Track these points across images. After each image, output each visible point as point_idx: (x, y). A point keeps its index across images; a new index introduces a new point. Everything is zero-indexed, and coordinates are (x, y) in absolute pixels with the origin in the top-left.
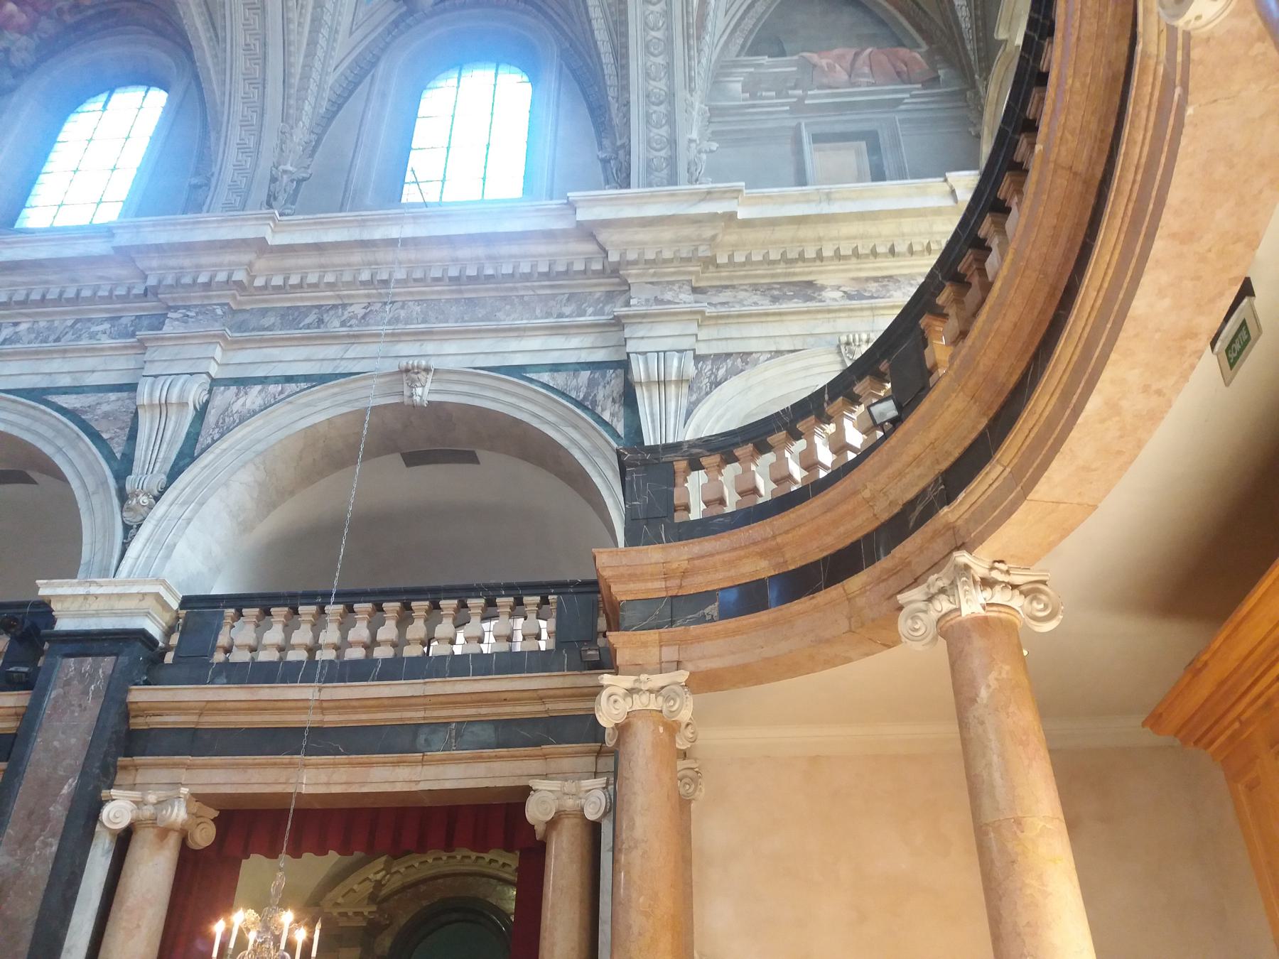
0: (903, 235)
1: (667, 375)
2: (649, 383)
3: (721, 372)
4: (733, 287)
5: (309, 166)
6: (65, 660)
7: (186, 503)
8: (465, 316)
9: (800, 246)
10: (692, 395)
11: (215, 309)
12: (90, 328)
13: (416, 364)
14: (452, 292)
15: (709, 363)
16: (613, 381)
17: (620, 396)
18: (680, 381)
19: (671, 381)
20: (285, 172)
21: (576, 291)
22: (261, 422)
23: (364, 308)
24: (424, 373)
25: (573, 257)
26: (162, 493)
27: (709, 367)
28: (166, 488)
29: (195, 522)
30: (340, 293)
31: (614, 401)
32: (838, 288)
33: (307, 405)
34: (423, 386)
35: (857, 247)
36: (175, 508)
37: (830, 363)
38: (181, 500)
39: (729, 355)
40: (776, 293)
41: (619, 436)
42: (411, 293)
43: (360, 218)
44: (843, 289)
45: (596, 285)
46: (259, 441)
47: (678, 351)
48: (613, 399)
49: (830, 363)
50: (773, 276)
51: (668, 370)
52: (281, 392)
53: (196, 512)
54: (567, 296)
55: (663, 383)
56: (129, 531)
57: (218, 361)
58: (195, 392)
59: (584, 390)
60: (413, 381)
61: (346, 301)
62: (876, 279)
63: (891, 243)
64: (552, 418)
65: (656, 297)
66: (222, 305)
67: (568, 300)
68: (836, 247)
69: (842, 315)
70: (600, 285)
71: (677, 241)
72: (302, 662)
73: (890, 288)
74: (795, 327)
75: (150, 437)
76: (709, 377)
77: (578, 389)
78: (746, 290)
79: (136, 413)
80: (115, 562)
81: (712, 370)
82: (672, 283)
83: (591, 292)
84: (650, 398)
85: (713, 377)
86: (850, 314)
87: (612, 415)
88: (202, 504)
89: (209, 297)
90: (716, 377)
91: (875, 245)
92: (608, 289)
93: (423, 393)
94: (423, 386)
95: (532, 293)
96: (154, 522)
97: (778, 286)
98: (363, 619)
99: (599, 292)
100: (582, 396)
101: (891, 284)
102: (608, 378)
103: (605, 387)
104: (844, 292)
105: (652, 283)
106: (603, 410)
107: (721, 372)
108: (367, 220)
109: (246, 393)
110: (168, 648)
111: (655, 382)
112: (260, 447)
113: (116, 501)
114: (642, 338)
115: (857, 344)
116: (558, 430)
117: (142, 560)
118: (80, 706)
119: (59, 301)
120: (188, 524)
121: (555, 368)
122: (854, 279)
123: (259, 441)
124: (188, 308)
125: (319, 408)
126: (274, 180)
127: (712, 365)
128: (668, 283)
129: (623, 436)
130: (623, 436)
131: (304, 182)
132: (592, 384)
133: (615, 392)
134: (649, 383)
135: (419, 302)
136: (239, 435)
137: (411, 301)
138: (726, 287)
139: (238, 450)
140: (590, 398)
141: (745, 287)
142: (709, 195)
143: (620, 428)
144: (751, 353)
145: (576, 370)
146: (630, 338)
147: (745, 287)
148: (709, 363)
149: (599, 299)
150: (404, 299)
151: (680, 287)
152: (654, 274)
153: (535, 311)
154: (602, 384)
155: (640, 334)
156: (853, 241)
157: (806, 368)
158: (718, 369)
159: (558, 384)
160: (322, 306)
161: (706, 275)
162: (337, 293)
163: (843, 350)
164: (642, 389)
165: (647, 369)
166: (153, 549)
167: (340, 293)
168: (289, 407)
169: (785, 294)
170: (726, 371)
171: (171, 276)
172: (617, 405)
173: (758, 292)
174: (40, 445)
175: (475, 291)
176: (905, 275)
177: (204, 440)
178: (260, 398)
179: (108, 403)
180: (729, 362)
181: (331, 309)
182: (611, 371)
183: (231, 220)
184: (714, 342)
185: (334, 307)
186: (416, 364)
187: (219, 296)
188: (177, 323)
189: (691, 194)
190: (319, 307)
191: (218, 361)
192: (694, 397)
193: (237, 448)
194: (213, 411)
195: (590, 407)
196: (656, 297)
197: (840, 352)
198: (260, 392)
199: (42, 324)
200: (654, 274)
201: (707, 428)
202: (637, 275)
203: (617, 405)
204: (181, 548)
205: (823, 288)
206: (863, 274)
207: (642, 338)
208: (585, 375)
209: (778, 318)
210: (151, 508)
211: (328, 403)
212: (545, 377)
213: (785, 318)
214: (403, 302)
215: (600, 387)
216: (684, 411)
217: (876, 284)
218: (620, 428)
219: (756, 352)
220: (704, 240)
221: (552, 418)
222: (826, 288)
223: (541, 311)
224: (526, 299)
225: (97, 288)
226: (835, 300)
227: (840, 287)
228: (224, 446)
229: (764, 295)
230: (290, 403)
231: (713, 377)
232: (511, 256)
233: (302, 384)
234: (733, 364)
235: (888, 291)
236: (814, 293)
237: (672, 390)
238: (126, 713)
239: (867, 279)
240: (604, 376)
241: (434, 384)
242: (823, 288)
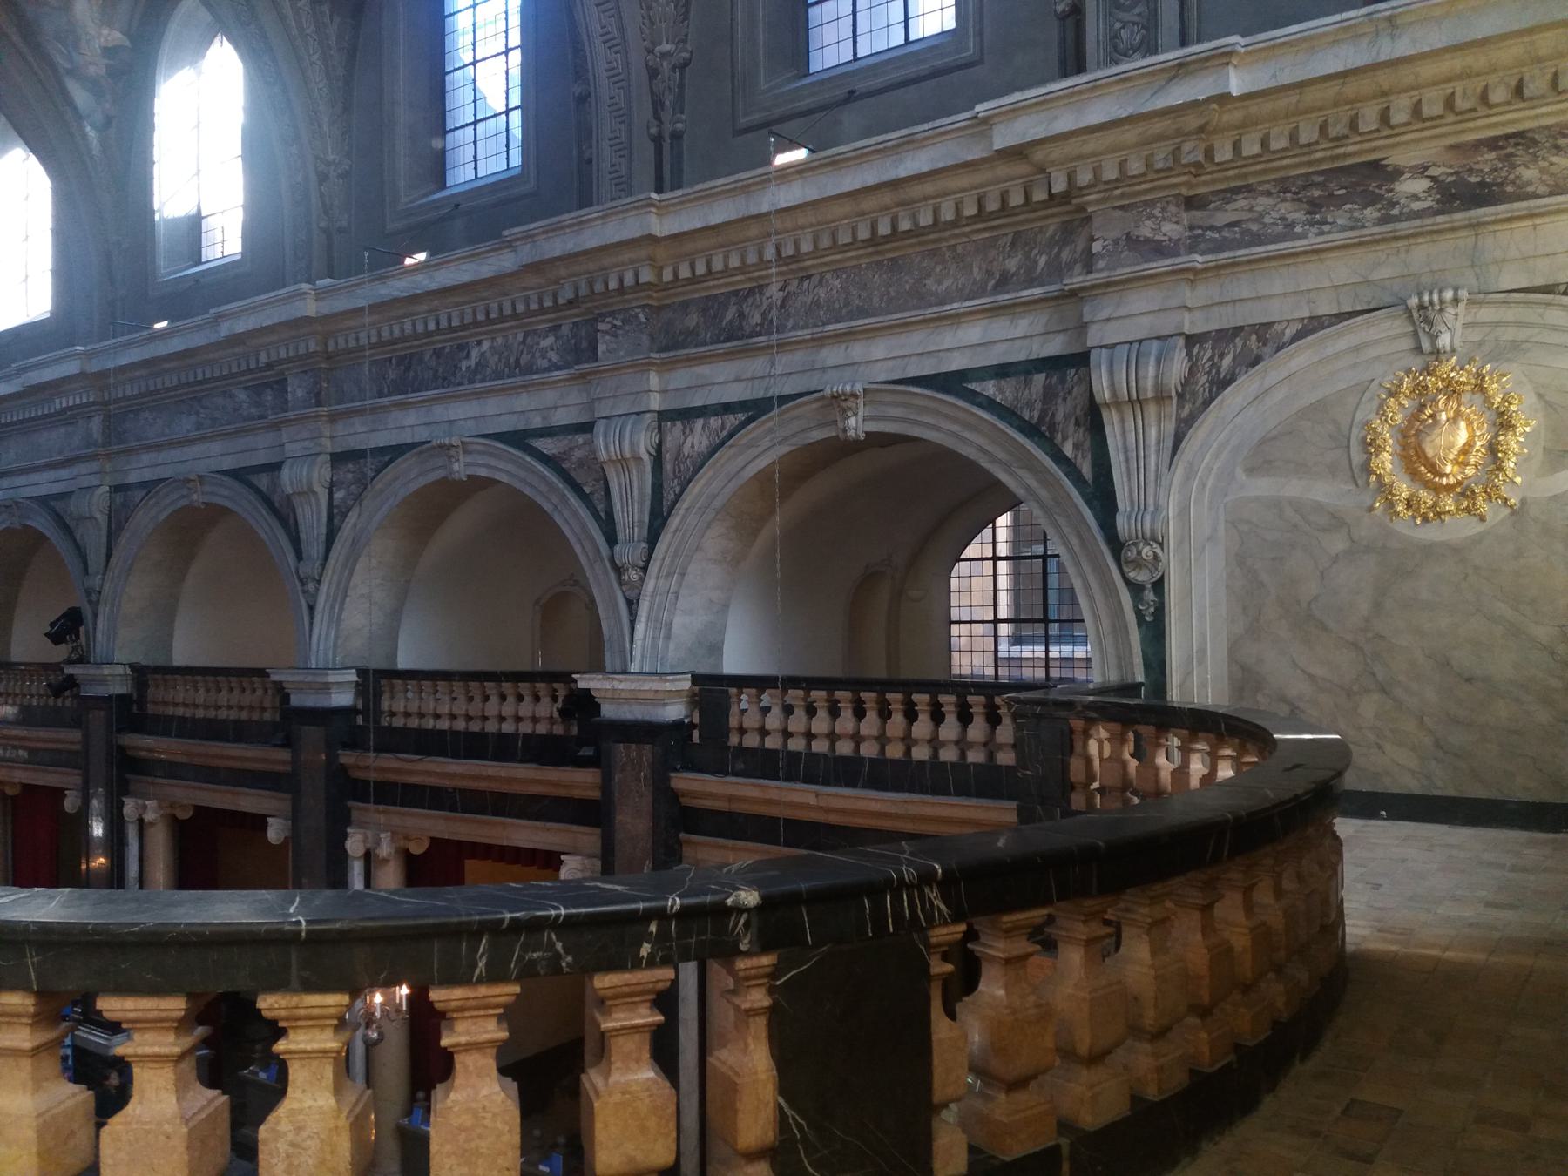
0: (1539, 60)
1: (1141, 392)
2: (1117, 403)
3: (1227, 362)
4: (1248, 189)
5: (686, 35)
6: (618, 745)
7: (669, 575)
8: (890, 289)
9: (1352, 109)
10: (1183, 407)
11: (637, 314)
12: (538, 344)
13: (840, 392)
14: (871, 254)
15: (1208, 345)
16: (1075, 389)
17: (1085, 414)
18: (1161, 397)
19: (1146, 400)
20: (664, 55)
21: (1021, 229)
22: (710, 473)
23: (780, 290)
24: (852, 399)
25: (1008, 184)
26: (648, 562)
27: (1209, 354)
28: (650, 555)
29: (683, 592)
30: (751, 275)
31: (1077, 424)
32: (1421, 170)
33: (749, 446)
34: (856, 415)
35: (1453, 94)
36: (661, 581)
37: (1396, 337)
38: (665, 570)
39: (1238, 330)
40: (1317, 193)
41: (1085, 482)
42: (825, 264)
43: (740, 184)
44: (1431, 172)
45: (1046, 217)
46: (715, 496)
47: (1158, 338)
48: (1076, 419)
49: (1396, 337)
50: (1310, 163)
51: (1141, 383)
52: (723, 428)
53: (680, 584)
54: (1010, 236)
55: (1137, 402)
56: (632, 604)
57: (656, 391)
58: (644, 443)
59: (1038, 405)
60: (844, 411)
61: (762, 282)
62: (1492, 144)
63: (1518, 77)
64: (1001, 455)
65: (1128, 234)
66: (643, 307)
67: (1013, 244)
68: (1415, 100)
69: (1420, 240)
70: (1053, 216)
71: (1146, 142)
72: (800, 753)
73: (1518, 160)
74: (1342, 269)
75: (621, 496)
76: (1209, 373)
77: (1030, 405)
78: (1268, 194)
79: (603, 468)
80: (628, 646)
81: (1211, 358)
82: (1150, 204)
83: (1041, 227)
84: (1122, 421)
85: (1214, 372)
86: (1435, 237)
87: (1076, 446)
88: (683, 575)
89: (629, 301)
90: (1218, 372)
91: (1486, 86)
92: (1066, 218)
93: (857, 423)
94: (856, 415)
95: (967, 240)
96: (648, 598)
97: (1321, 179)
98: (846, 707)
99: (1052, 227)
100: (1036, 414)
101: (1520, 151)
102: (1068, 385)
103: (1065, 399)
104: (1433, 179)
105: (1121, 208)
106: (1065, 439)
107: (1227, 362)
108: (750, 185)
109: (691, 431)
110: (692, 726)
111: (1125, 402)
112: (717, 503)
113: (612, 575)
114: (1108, 320)
115: (1438, 307)
116: (1012, 474)
117: (649, 641)
118: (637, 792)
119: (502, 319)
120: (677, 598)
121: (1002, 371)
122: (1452, 147)
123: (715, 496)
124: (612, 314)
125: (761, 449)
126: (653, 73)
127: (1213, 349)
128: (1146, 203)
129: (1090, 481)
130: (1090, 481)
131: (687, 69)
132: (1049, 395)
133: (1079, 407)
134: (1117, 403)
135: (837, 272)
136: (696, 490)
137: (828, 271)
138: (1237, 191)
139: (700, 508)
140: (1048, 419)
141: (1267, 186)
142: (1181, 69)
143: (1086, 470)
144: (1270, 324)
145: (1028, 373)
146: (1093, 322)
147: (1267, 186)
148: (1208, 345)
149: (1052, 237)
150: (820, 270)
151: (1163, 210)
152: (1123, 196)
153: (971, 270)
154: (1061, 394)
155: (1104, 314)
156: (1445, 86)
157: (1357, 349)
158: (1222, 356)
159: (1006, 400)
160: (739, 291)
161: (1203, 178)
162: (747, 276)
163: (1415, 315)
164: (1110, 411)
165: (1112, 385)
166: (655, 628)
167: (751, 275)
168: (732, 451)
169: (1331, 195)
170: (1234, 359)
171: (584, 282)
172: (1081, 430)
173: (1289, 195)
174: (539, 500)
175: (895, 249)
176: (1548, 127)
177: (669, 496)
178: (705, 437)
179: (579, 447)
180: (1239, 342)
181: (748, 295)
182: (1073, 371)
183: (612, 214)
184: (1216, 309)
185: (751, 290)
186: (840, 392)
187: (637, 299)
188: (608, 337)
189: (1153, 73)
190: (736, 293)
191: (656, 391)
192: (1185, 412)
193: (698, 505)
194: (668, 456)
195: (1047, 434)
196: (1128, 234)
197: (1411, 317)
198: (704, 427)
199: (500, 340)
200: (1123, 196)
201: (1203, 465)
202: (1098, 202)
203: (1081, 430)
204: (678, 621)
205: (1397, 173)
206: (1470, 137)
207: (1108, 320)
208: (1039, 379)
209: (1314, 257)
210: (642, 580)
211: (766, 443)
212: (989, 388)
213: (1323, 256)
214: (821, 274)
215: (1060, 401)
216: (1169, 443)
217: (1493, 155)
218: (1086, 470)
219: (1280, 322)
220: (1189, 134)
221: (1001, 455)
222: (1402, 174)
223: (980, 269)
224: (960, 249)
225: (527, 300)
226: (1415, 197)
227: (1427, 168)
228: (686, 505)
229: (1299, 200)
230: (731, 446)
231: (1214, 372)
232: (926, 198)
233: (740, 415)
234: (1244, 345)
235: (1513, 166)
236: (1380, 187)
237: (1152, 410)
238: (674, 796)
239: (1478, 145)
240: (1063, 381)
241: (867, 408)
242: (1397, 173)
